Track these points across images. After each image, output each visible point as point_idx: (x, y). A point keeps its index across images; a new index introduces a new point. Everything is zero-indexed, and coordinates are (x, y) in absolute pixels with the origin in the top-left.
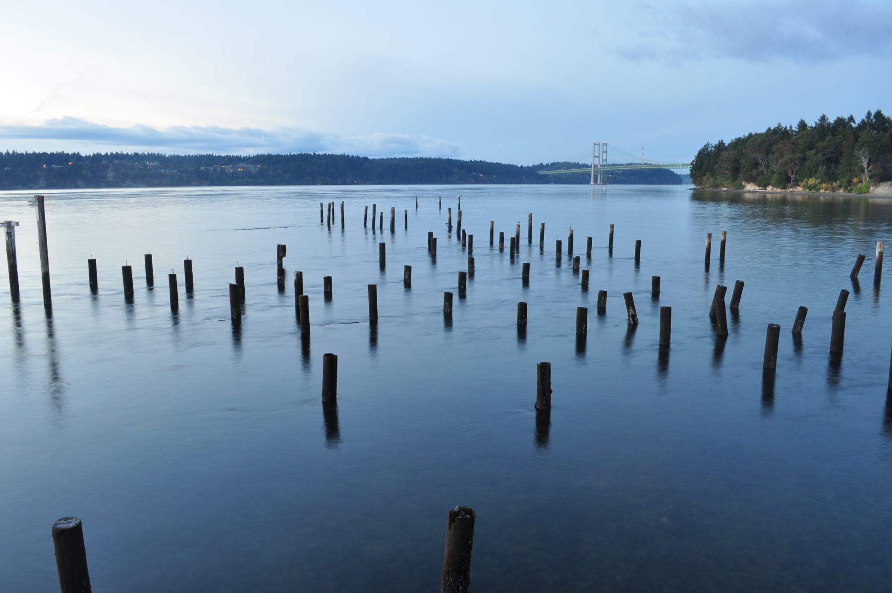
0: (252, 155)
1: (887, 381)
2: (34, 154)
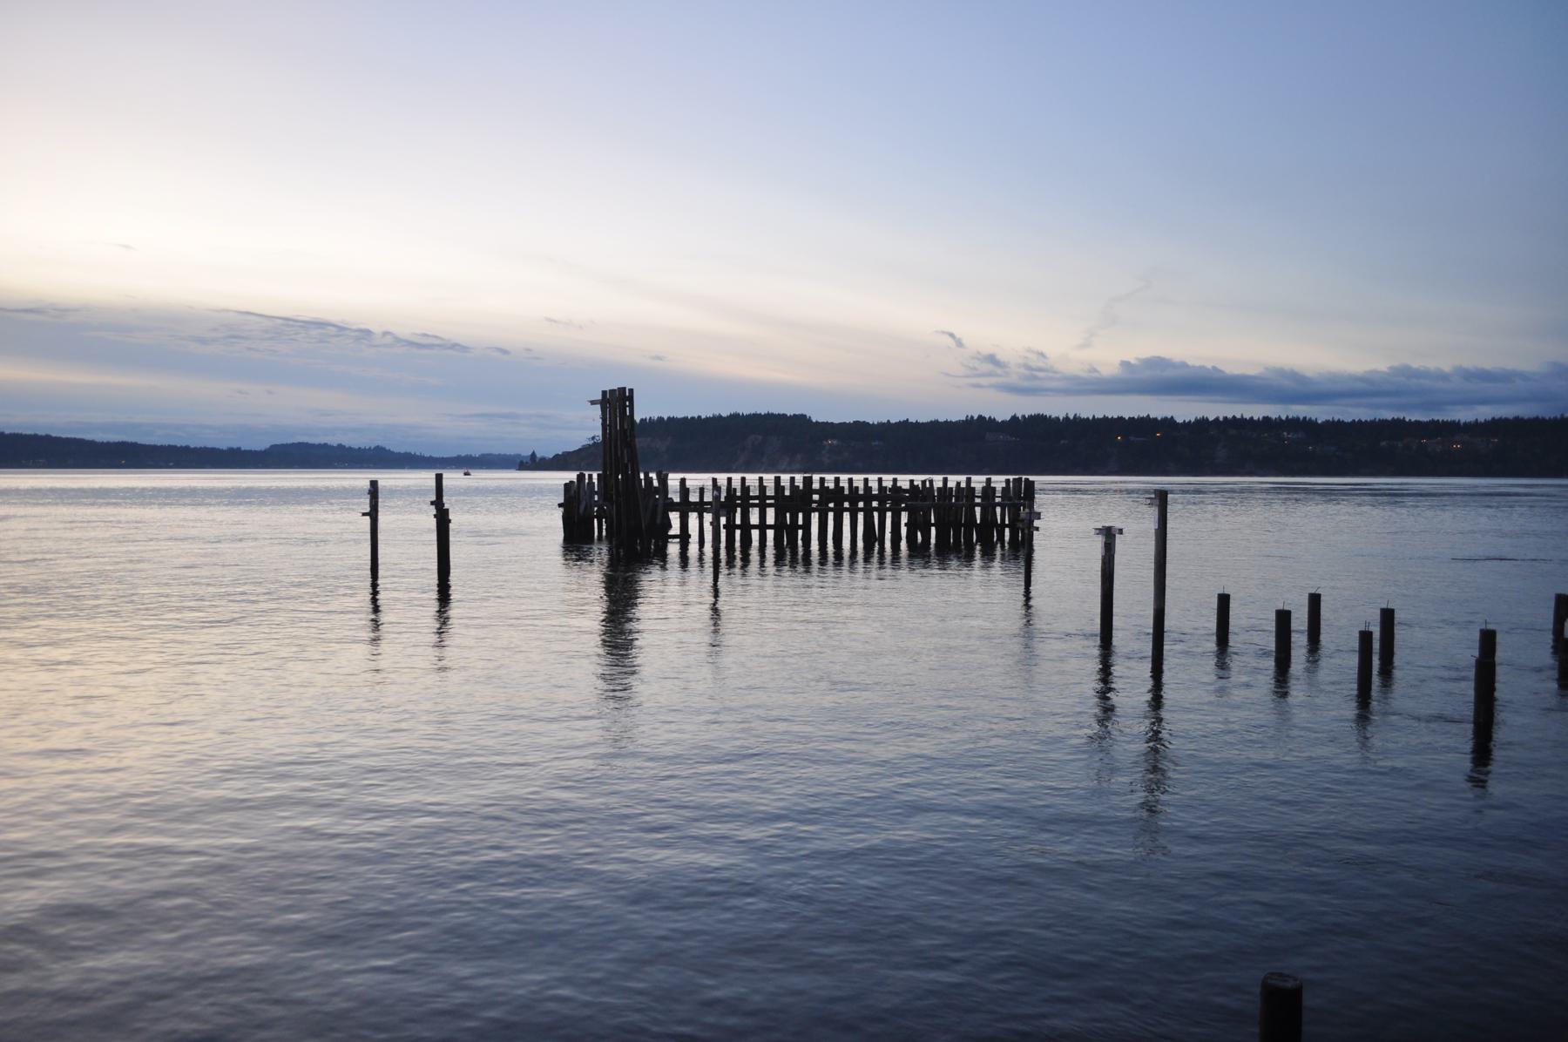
0: (1481, 419)
1: (1498, 669)
2: (1105, 419)
